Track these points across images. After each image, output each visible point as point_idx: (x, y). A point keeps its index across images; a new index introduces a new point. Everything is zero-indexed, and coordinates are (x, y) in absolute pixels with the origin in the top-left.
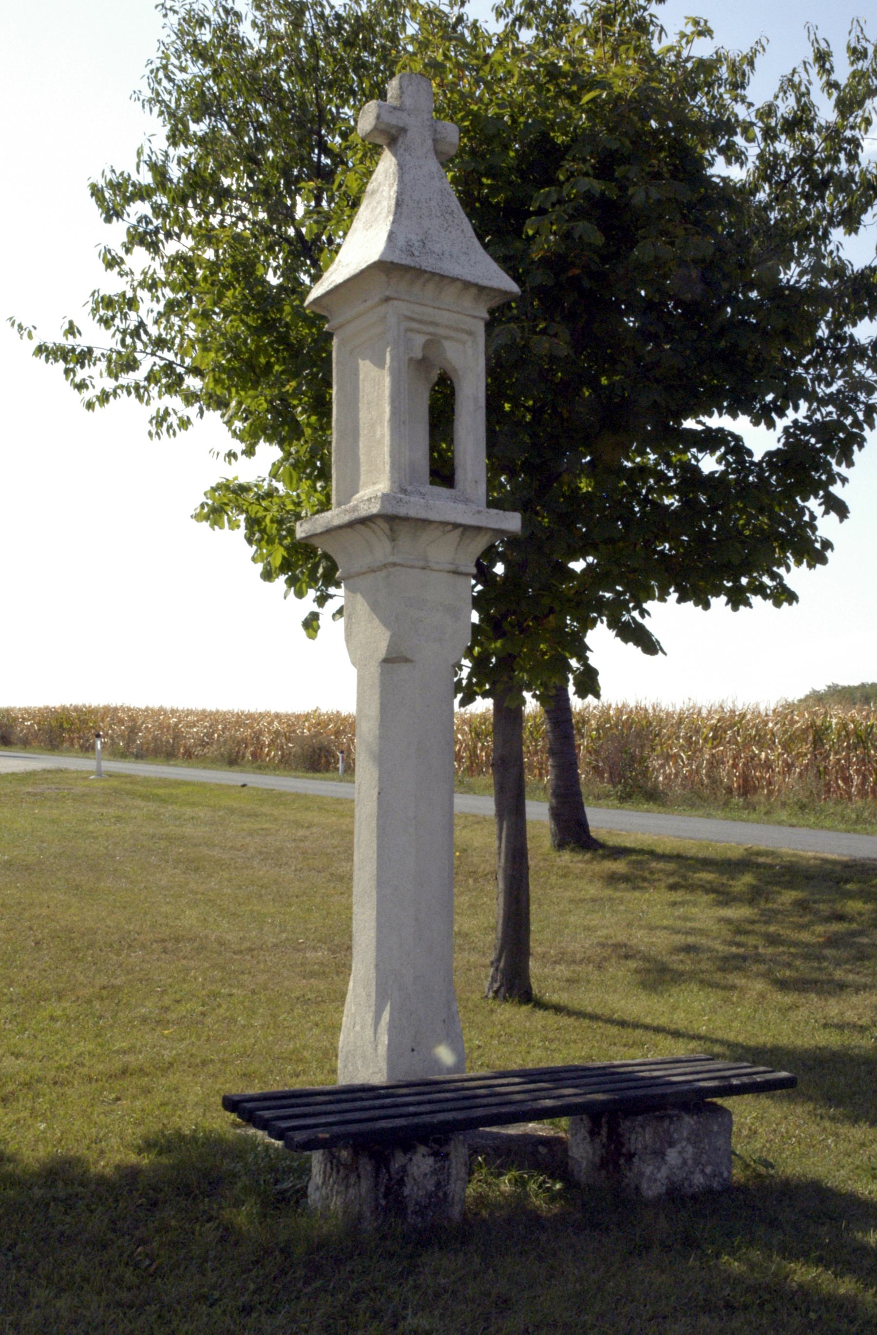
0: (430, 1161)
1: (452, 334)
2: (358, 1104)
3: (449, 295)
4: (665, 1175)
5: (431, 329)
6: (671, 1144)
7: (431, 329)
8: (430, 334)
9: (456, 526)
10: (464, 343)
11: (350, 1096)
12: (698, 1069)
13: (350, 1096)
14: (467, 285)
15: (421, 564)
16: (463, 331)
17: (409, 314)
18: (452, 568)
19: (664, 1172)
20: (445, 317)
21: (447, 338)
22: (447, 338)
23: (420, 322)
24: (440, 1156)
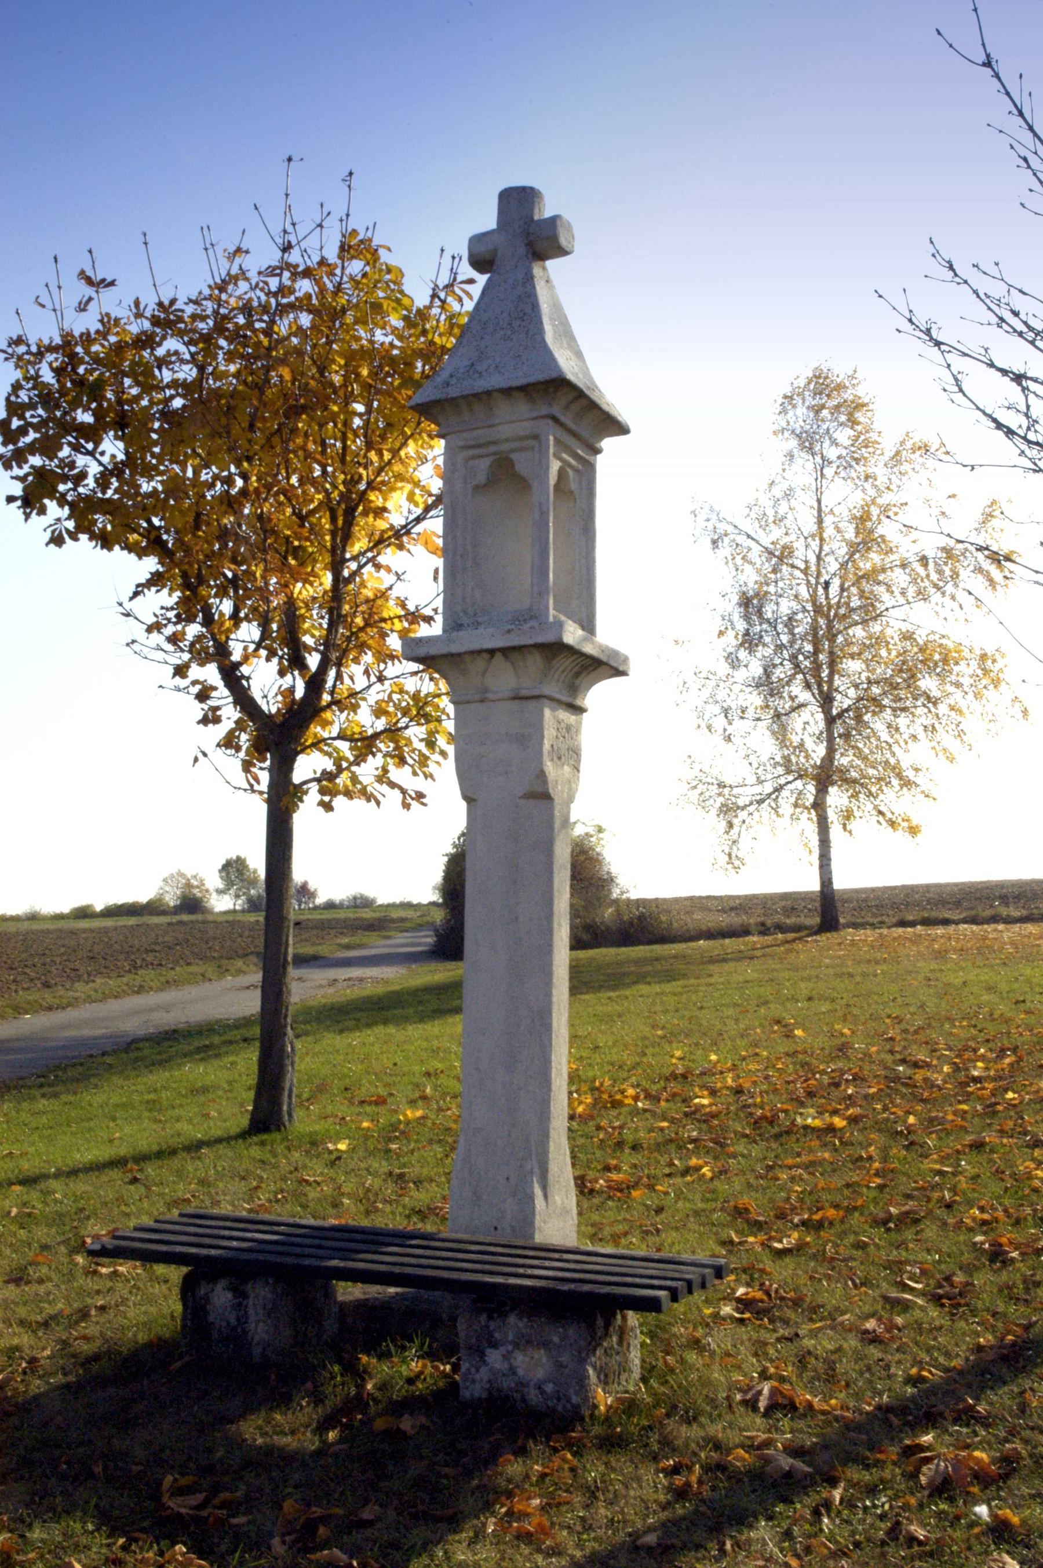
0: (230, 1295)
1: (516, 445)
2: (547, 1263)
3: (503, 409)
4: (485, 1379)
5: (492, 449)
6: (494, 1345)
7: (492, 449)
8: (494, 454)
9: (480, 652)
10: (533, 448)
11: (346, 1235)
12: (670, 1274)
13: (346, 1235)
14: (508, 392)
15: (477, 697)
16: (527, 438)
17: (462, 444)
18: (512, 694)
19: (484, 1374)
20: (506, 431)
21: (513, 451)
22: (513, 451)
23: (479, 446)
24: (240, 1294)
